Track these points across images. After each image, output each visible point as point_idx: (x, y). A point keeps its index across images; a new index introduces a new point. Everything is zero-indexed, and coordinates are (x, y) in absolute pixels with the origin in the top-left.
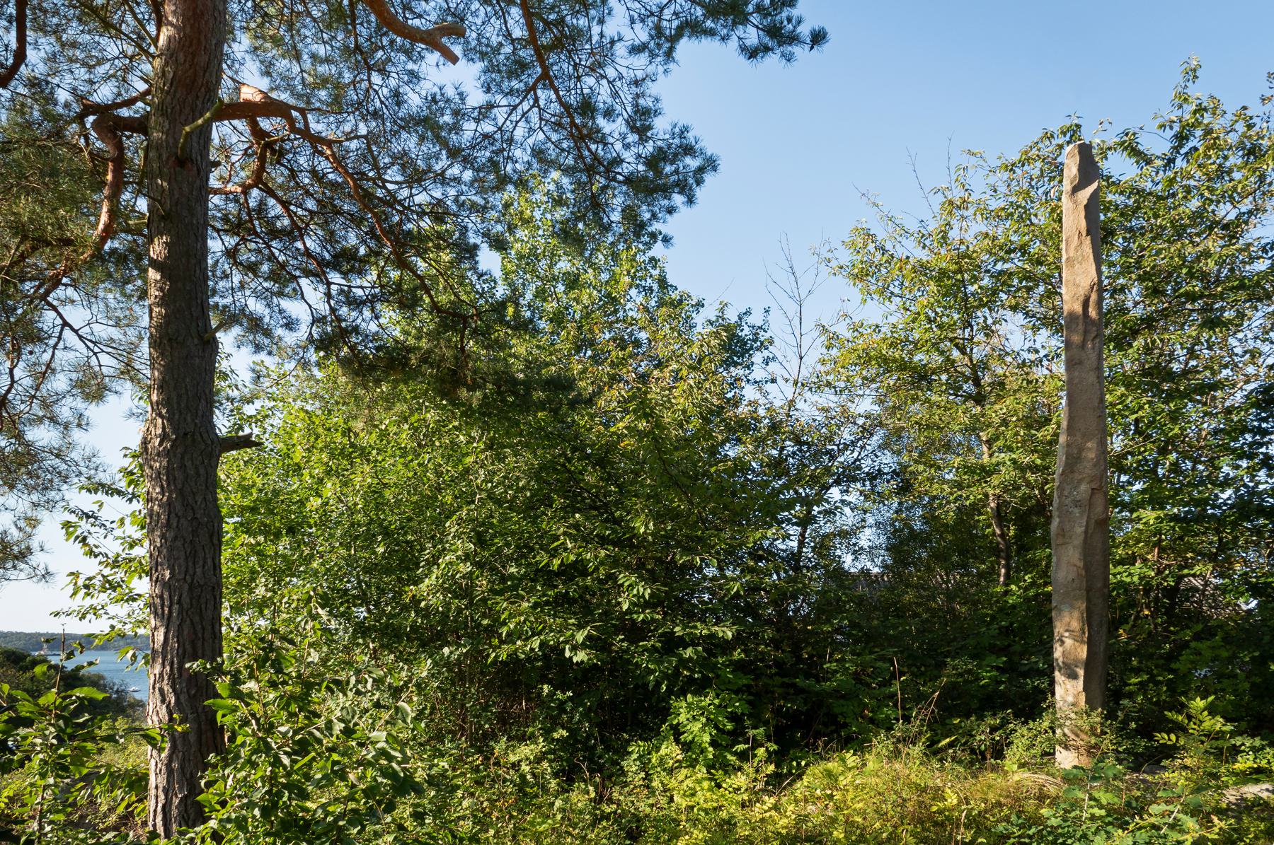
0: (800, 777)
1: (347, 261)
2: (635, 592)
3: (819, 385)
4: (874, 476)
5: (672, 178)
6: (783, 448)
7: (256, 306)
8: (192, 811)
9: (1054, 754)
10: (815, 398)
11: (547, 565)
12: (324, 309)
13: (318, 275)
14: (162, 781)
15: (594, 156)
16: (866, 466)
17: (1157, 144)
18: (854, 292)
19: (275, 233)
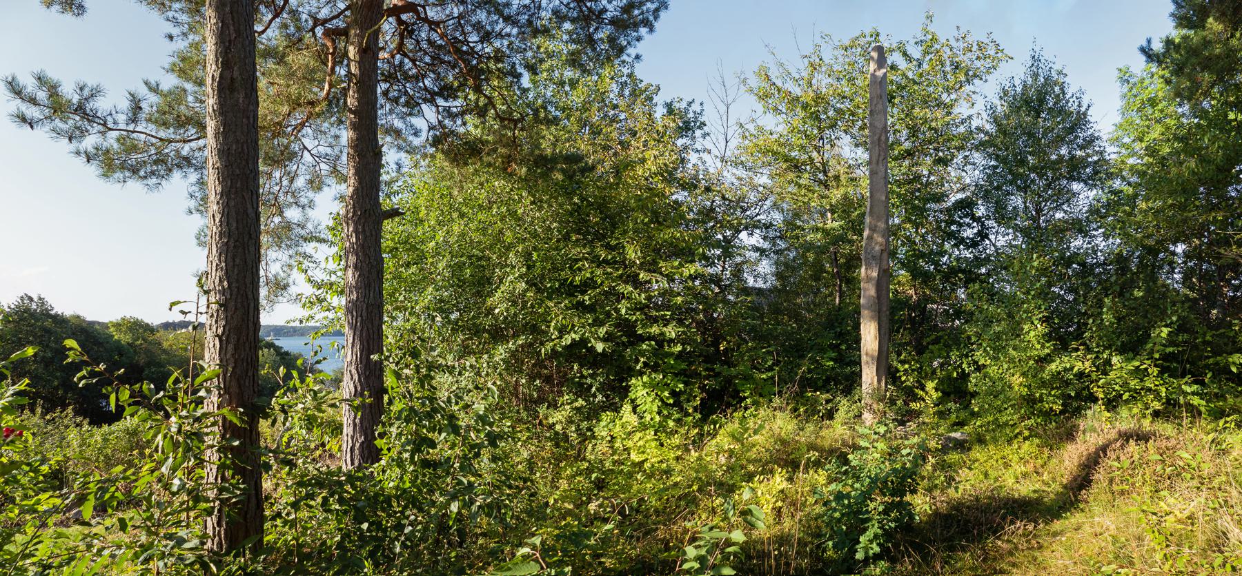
0: (714, 436)
1: (447, 91)
3: (736, 163)
7: (398, 124)
8: (370, 452)
10: (735, 171)
11: (572, 282)
12: (434, 121)
13: (432, 101)
14: (351, 433)
15: (590, 9)
17: (916, 52)
19: (407, 78)
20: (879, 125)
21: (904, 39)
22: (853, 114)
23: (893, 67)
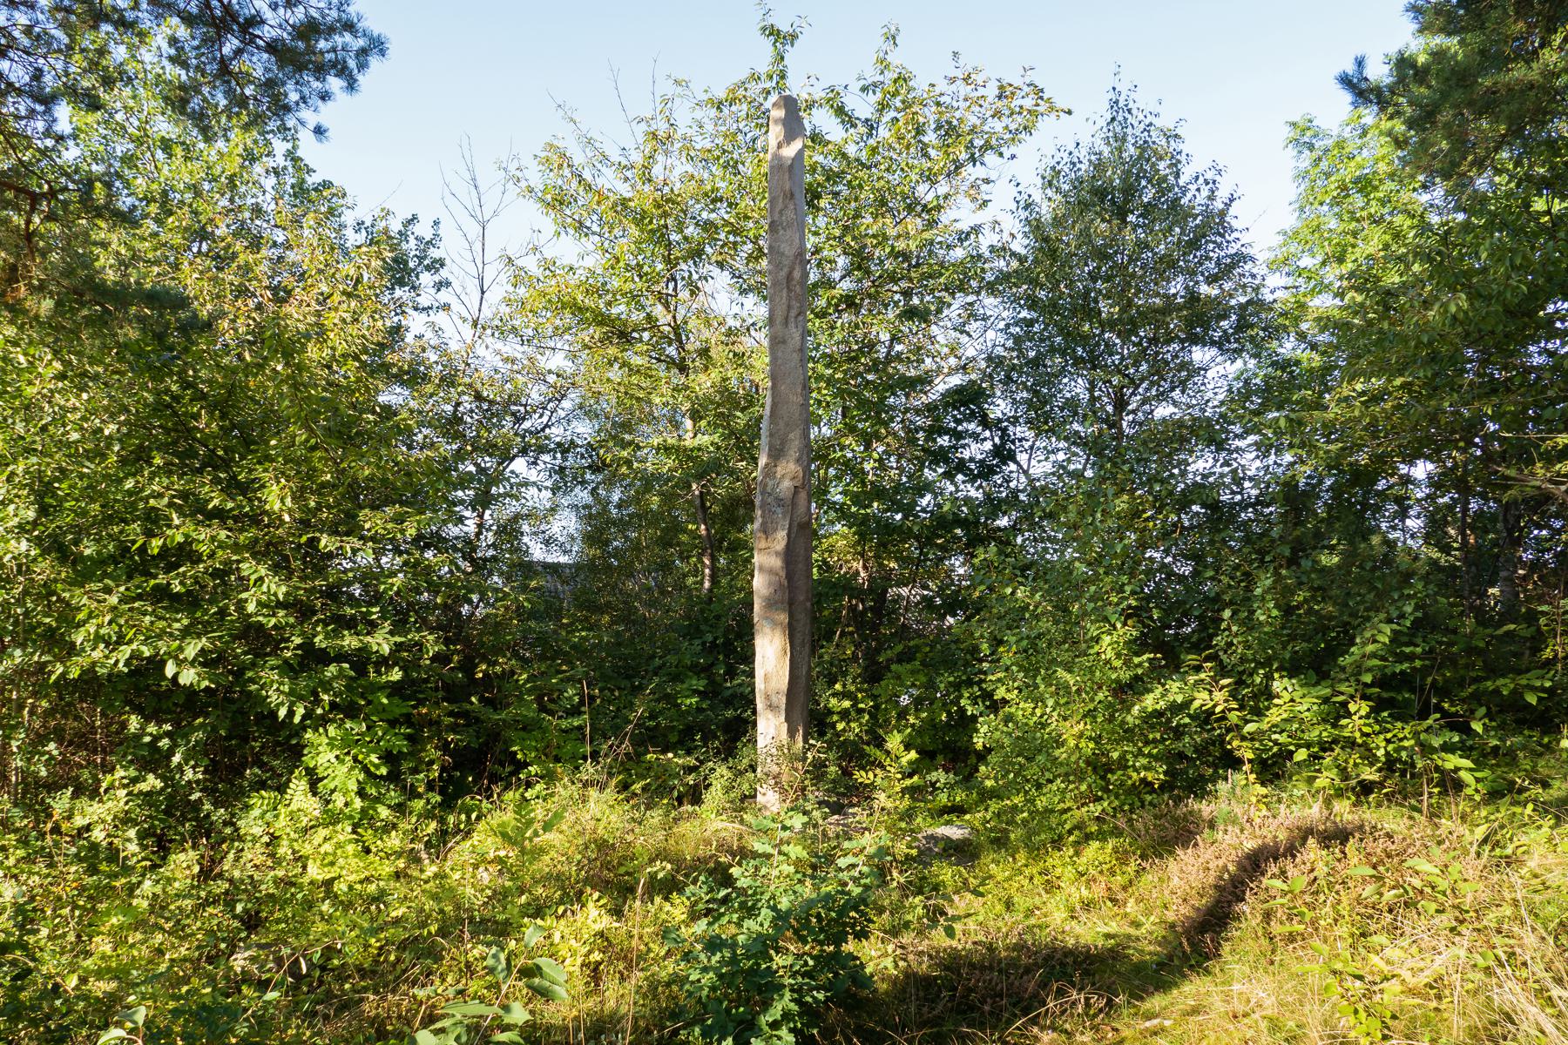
2: (264, 588)
3: (504, 330)
4: (565, 448)
5: (328, 56)
6: (458, 404)
9: (755, 796)
10: (499, 345)
16: (556, 433)
17: (863, 107)
18: (547, 223)
20: (789, 250)
21: (838, 81)
22: (735, 232)
23: (817, 138)
